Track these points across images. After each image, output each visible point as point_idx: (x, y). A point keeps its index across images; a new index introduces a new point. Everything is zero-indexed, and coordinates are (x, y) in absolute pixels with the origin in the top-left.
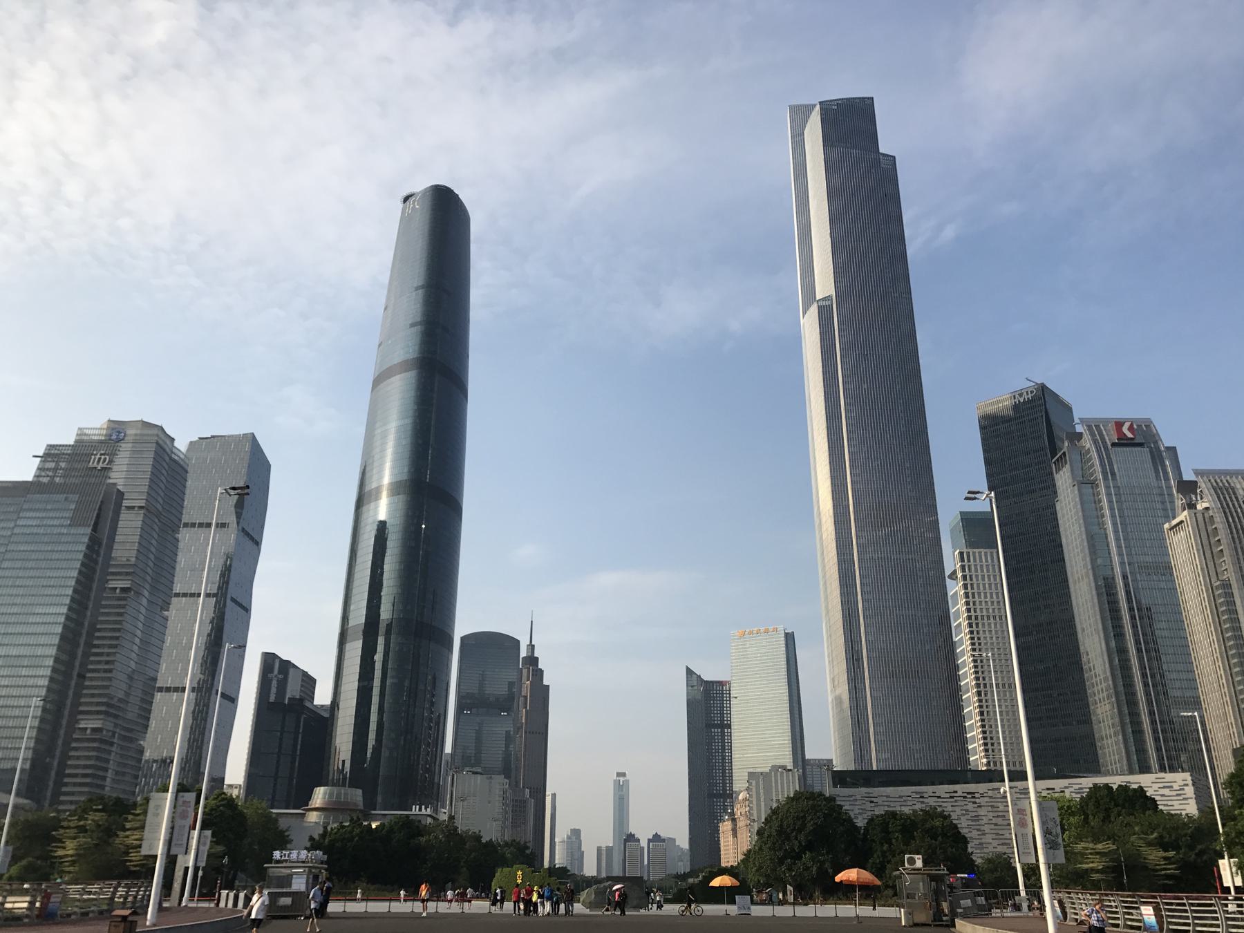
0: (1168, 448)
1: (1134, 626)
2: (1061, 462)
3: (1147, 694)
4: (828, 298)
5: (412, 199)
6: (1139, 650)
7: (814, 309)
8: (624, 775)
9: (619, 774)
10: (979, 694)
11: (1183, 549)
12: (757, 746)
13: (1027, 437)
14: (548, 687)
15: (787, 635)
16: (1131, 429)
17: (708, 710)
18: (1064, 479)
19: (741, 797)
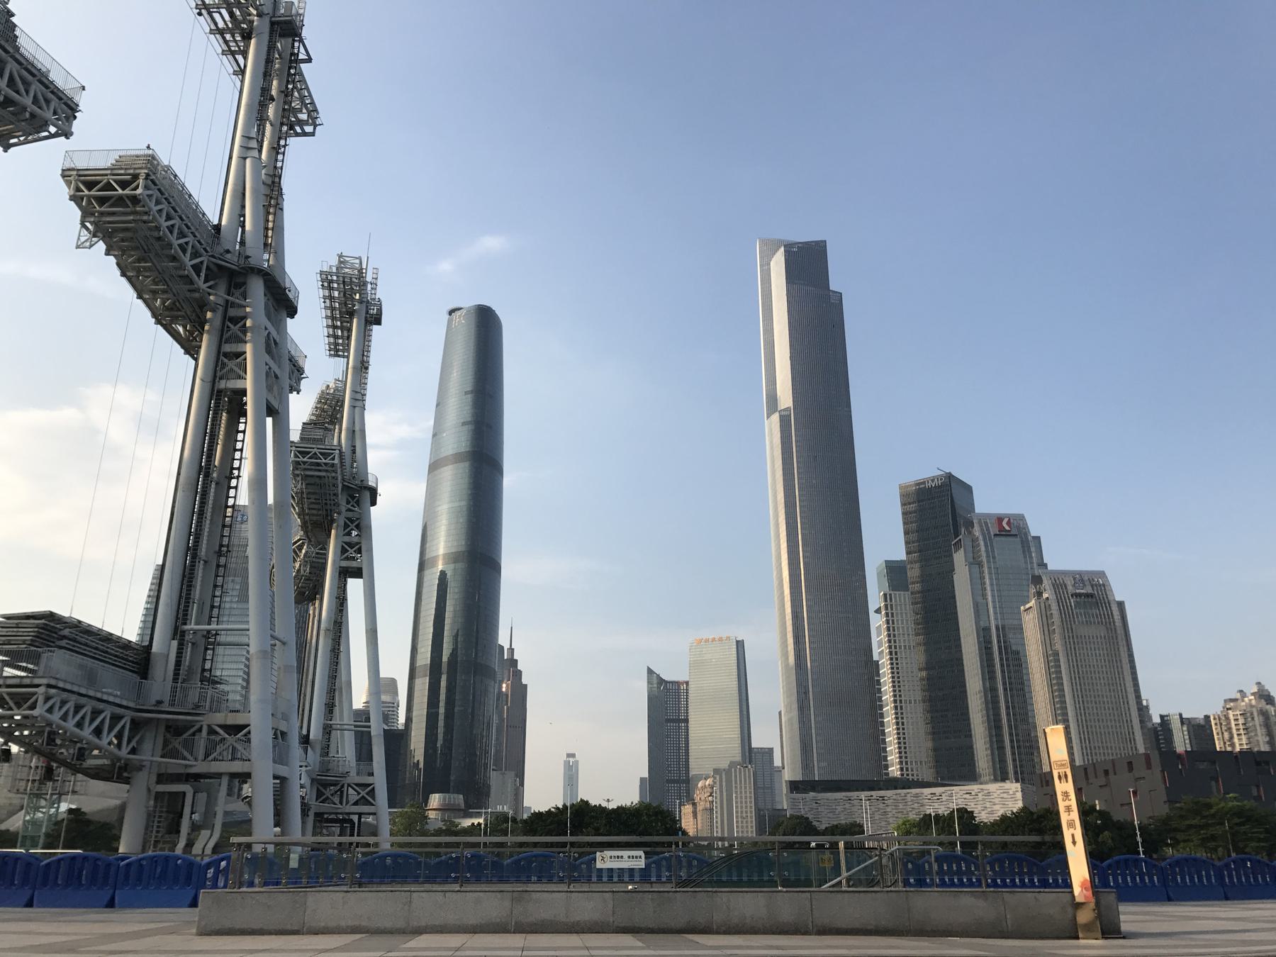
0: (1034, 538)
1: (1003, 672)
2: (958, 545)
3: (1009, 720)
4: (788, 409)
5: (458, 313)
6: (1005, 689)
7: (776, 417)
8: (573, 755)
9: (569, 755)
10: (896, 708)
11: (1030, 623)
12: (711, 739)
13: (938, 510)
14: (526, 686)
15: (738, 642)
16: (1008, 523)
17: (667, 709)
18: (959, 558)
19: (700, 785)
